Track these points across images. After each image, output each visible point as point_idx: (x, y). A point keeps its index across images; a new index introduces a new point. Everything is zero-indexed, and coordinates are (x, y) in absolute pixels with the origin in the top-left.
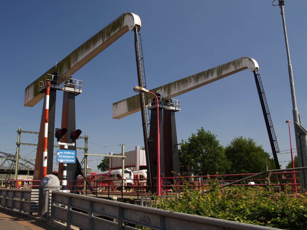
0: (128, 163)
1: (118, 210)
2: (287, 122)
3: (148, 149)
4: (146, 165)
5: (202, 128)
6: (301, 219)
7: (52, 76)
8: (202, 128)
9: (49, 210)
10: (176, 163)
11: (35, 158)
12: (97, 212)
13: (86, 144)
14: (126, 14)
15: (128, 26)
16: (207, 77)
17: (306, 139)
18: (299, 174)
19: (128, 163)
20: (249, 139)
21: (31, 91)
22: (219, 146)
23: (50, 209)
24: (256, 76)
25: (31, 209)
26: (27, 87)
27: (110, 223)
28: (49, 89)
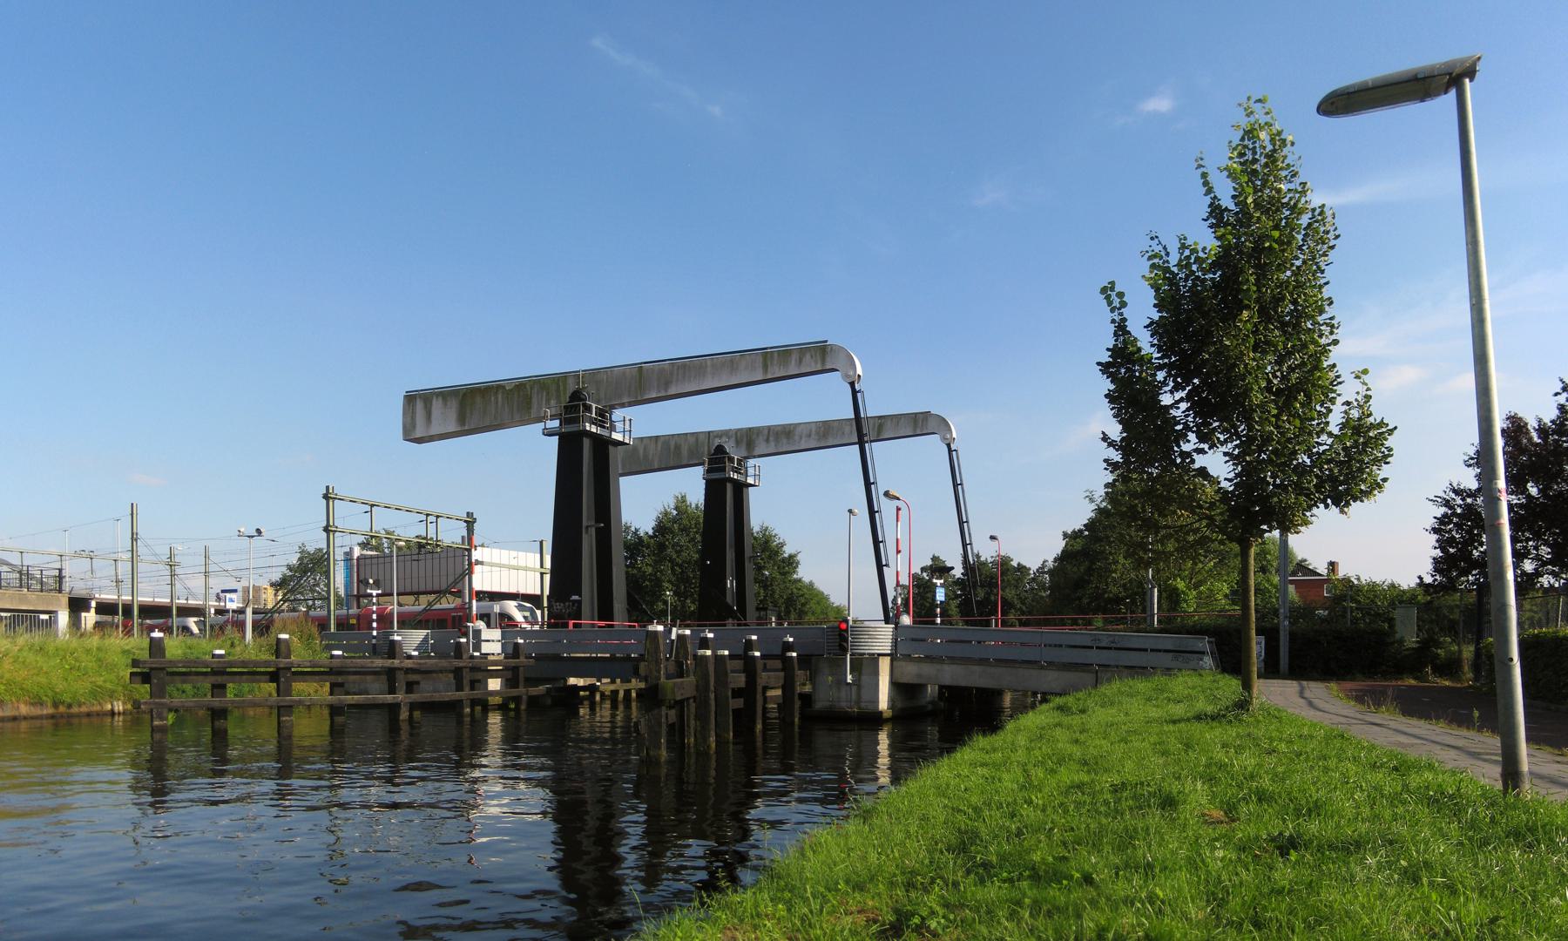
0: (436, 580)
1: (67, 613)
2: (993, 538)
3: (355, 670)
4: (499, 680)
5: (1105, 461)
6: (1105, 939)
7: (212, 697)
8: (1396, 428)
9: (600, 733)
10: (340, 679)
11: (498, 550)
12: (1324, 711)
13: (135, 543)
14: (740, 827)
15: (1318, 111)
16: (1450, 722)
17: (1373, 587)
18: (1546, 824)
19: (436, 580)
20: (1212, 728)
21: (402, 928)
22: (1438, 553)
23: (720, 652)
24: (854, 393)
25: (605, 612)
26: (1319, 101)
27: (1148, 598)
28: (662, 741)
